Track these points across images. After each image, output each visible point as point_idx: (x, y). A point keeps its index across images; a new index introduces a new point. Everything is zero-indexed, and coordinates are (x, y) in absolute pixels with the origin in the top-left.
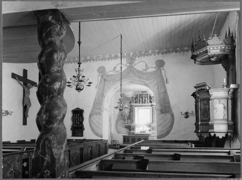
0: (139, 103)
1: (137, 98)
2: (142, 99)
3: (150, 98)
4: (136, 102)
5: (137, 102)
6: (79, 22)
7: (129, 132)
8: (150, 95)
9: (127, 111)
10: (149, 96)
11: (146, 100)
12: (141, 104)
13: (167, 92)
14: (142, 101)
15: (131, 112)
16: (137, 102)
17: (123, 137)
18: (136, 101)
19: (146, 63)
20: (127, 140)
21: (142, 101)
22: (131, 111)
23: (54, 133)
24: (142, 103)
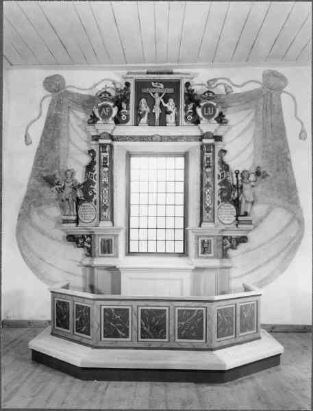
0: (163, 123)
1: (128, 102)
2: (151, 103)
3: (187, 103)
4: (117, 121)
5: (124, 117)
6: (131, 251)
7: (87, 261)
8: (188, 84)
9: (76, 162)
10: (183, 89)
11: (170, 108)
12: (144, 129)
13: (279, 73)
14: (151, 115)
15: (96, 167)
16: (127, 121)
17: (53, 298)
18: (119, 114)
19: (111, 80)
20: (73, 319)
21: (151, 115)
22: (101, 158)
23: (221, 103)
24: (151, 123)
